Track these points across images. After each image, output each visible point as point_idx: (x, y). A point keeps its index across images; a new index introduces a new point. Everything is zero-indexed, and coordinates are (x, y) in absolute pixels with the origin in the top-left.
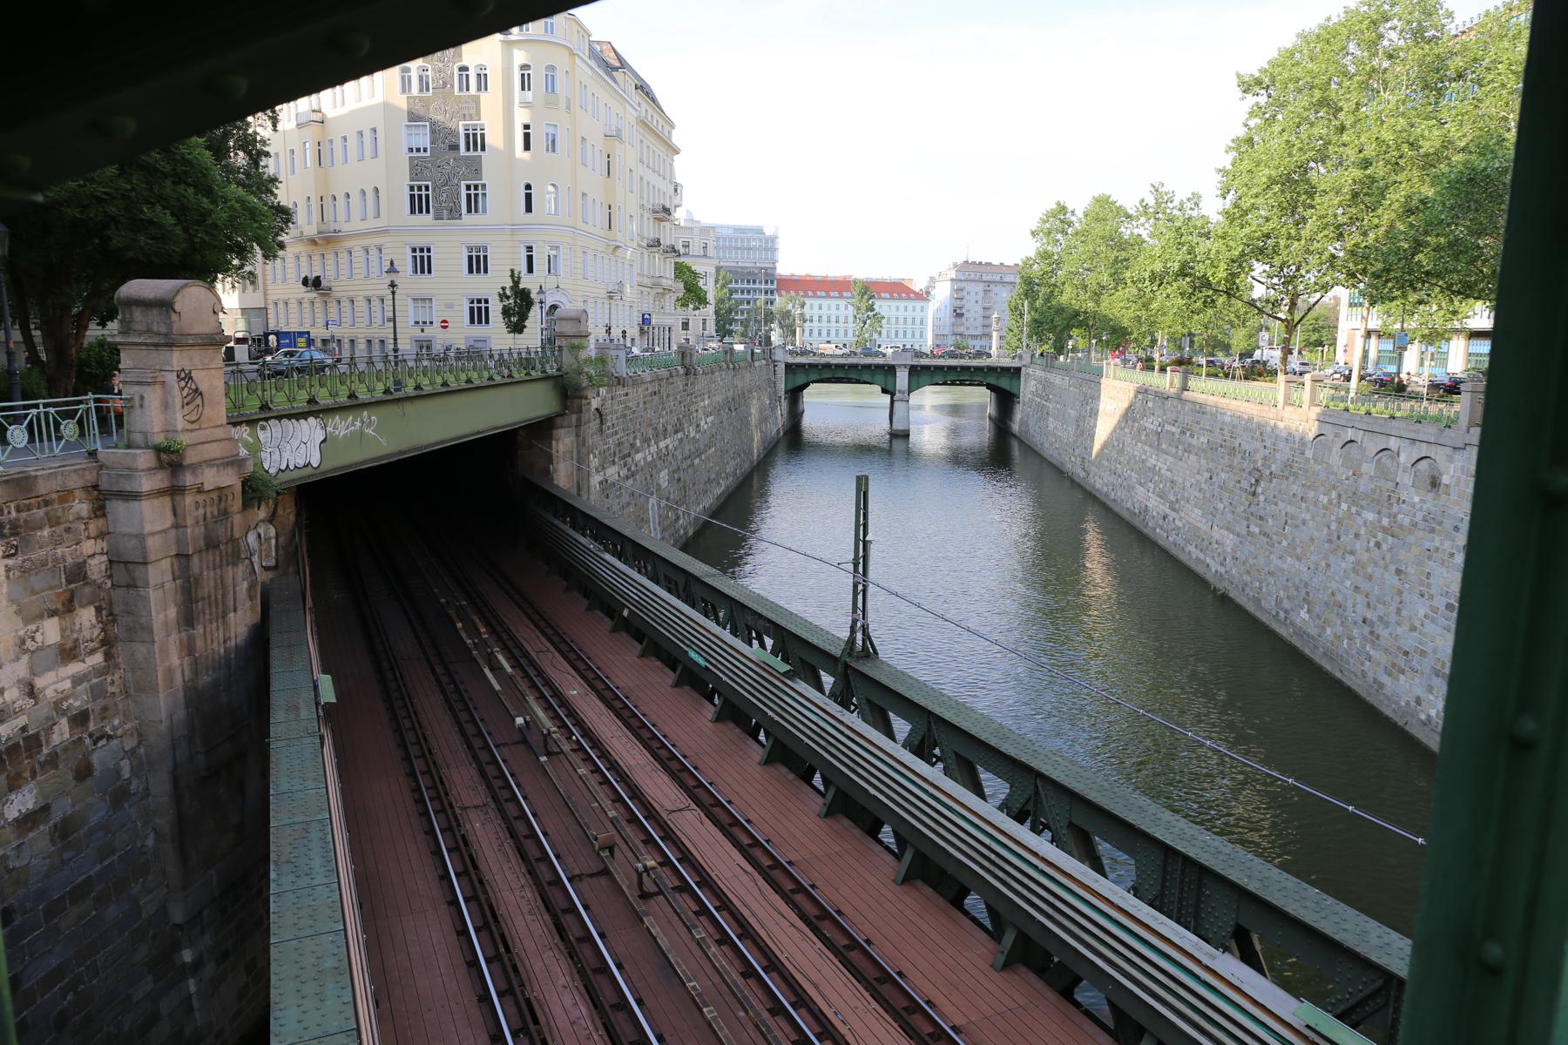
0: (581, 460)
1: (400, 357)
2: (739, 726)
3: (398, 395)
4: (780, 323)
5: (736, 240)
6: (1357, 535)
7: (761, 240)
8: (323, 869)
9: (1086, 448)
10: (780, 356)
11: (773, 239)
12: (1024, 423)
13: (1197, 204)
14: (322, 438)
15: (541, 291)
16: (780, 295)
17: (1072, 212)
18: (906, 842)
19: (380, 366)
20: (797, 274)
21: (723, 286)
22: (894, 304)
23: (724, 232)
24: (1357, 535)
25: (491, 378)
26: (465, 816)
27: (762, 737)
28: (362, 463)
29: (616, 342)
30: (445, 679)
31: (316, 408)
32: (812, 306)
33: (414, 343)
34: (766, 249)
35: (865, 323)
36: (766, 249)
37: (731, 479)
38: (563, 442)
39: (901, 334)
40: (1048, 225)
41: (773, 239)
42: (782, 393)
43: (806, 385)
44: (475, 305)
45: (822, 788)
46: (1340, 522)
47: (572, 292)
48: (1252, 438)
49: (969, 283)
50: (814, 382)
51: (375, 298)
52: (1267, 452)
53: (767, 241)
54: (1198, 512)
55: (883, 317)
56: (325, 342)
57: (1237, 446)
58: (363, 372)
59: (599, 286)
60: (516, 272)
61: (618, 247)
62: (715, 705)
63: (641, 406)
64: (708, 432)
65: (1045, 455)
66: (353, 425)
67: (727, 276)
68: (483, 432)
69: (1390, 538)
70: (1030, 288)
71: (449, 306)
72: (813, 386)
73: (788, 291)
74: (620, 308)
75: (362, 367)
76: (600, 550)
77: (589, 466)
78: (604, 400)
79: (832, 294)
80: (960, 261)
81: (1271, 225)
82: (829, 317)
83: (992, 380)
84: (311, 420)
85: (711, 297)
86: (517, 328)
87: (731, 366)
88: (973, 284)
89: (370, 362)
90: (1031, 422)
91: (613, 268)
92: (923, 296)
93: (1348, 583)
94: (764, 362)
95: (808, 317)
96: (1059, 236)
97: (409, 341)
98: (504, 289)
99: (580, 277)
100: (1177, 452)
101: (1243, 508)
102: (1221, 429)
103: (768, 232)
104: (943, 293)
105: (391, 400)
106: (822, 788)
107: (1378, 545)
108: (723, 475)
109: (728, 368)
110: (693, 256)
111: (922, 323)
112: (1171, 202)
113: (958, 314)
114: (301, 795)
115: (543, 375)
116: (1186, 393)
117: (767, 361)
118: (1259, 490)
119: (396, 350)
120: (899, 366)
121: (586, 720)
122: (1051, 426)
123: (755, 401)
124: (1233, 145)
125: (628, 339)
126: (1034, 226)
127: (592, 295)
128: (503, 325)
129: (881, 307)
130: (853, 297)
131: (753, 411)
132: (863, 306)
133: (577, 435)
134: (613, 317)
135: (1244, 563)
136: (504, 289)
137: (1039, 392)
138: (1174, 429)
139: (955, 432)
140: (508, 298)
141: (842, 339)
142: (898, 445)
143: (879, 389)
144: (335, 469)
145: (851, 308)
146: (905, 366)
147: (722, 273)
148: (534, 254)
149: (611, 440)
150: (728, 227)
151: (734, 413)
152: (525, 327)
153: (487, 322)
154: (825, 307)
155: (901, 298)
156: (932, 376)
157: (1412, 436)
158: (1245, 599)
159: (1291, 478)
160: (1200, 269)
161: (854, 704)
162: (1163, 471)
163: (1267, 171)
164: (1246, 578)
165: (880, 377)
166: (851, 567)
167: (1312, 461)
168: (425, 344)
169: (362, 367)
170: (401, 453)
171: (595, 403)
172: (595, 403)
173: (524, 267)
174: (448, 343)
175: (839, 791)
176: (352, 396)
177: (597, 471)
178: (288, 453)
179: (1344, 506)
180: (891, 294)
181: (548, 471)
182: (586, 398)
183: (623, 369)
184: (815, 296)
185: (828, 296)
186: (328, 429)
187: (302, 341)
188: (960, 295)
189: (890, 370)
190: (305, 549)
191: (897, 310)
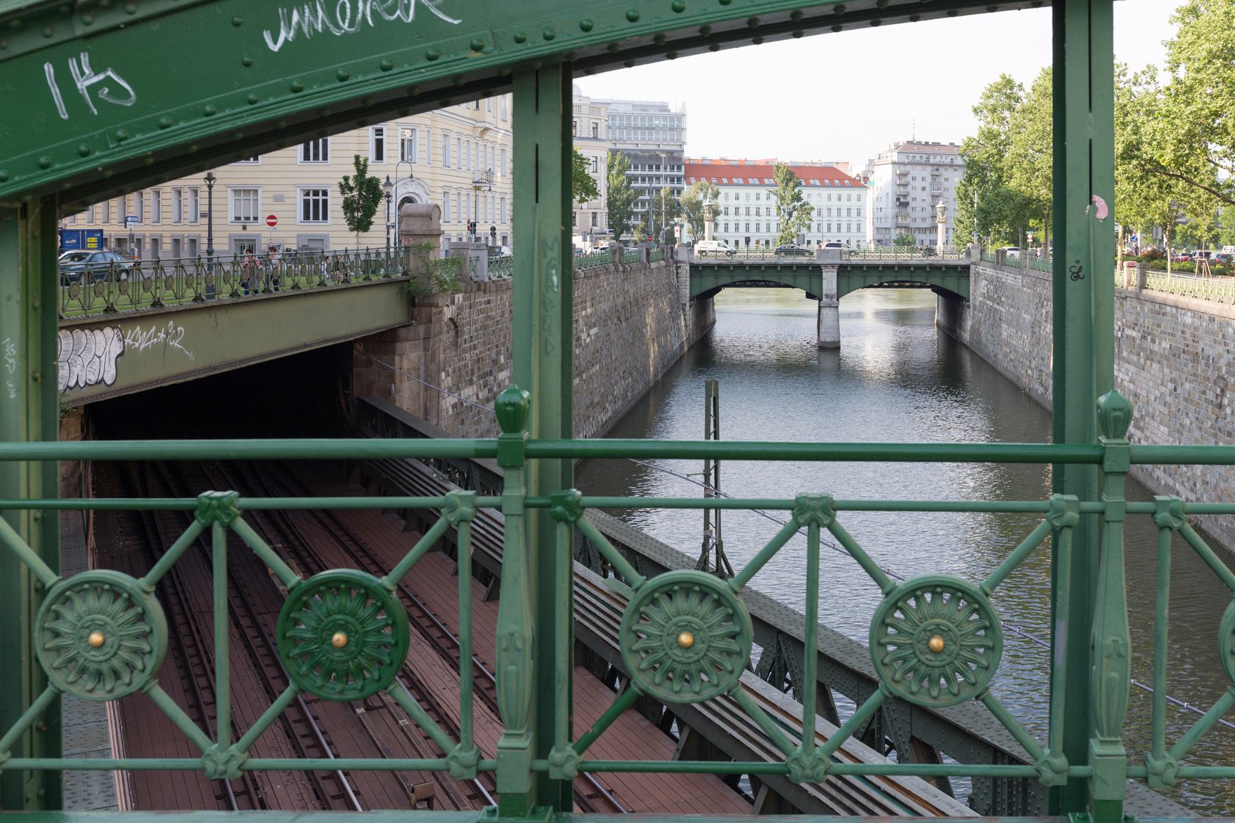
0: (430, 379)
1: (215, 260)
2: (592, 672)
3: (210, 303)
4: (689, 216)
5: (636, 118)
7: (665, 119)
8: (102, 794)
9: (1043, 359)
10: (682, 255)
11: (680, 117)
12: (975, 331)
13: (1153, 78)
14: (119, 351)
15: (388, 184)
16: (689, 183)
17: (1020, 86)
18: (685, 723)
19: (190, 270)
20: (692, 157)
21: (620, 173)
22: (825, 192)
23: (621, 109)
25: (322, 284)
26: (264, 778)
27: (675, 728)
28: (165, 380)
29: (483, 241)
30: (260, 652)
31: (114, 317)
32: (727, 195)
33: (233, 244)
35: (790, 215)
36: (671, 129)
37: (620, 402)
38: (408, 357)
39: (834, 228)
40: (992, 101)
41: (680, 117)
42: (686, 300)
43: (717, 290)
44: (311, 197)
45: (750, 793)
47: (429, 182)
48: (1215, 341)
49: (914, 167)
51: (186, 189)
53: (672, 119)
54: (1164, 429)
55: (812, 209)
56: (120, 241)
57: (1199, 350)
58: (170, 276)
59: (464, 175)
60: (361, 159)
61: (486, 129)
62: (615, 690)
63: (507, 315)
64: (591, 347)
65: (999, 369)
66: (156, 336)
67: (622, 160)
68: (310, 345)
70: (975, 170)
71: (279, 199)
72: (726, 291)
73: (698, 179)
74: (490, 200)
75: (170, 271)
76: (444, 480)
77: (439, 386)
78: (460, 308)
79: (735, 180)
80: (902, 140)
81: (1220, 102)
82: (748, 209)
83: (936, 281)
84: (108, 331)
85: (602, 187)
86: (361, 225)
88: (919, 167)
89: (179, 266)
90: (983, 330)
91: (481, 154)
92: (859, 183)
94: (663, 263)
95: (722, 209)
96: (1007, 114)
97: (227, 241)
98: (346, 179)
99: (440, 165)
100: (1139, 361)
101: (1210, 423)
102: (1183, 332)
103: (674, 109)
104: (884, 178)
105: (203, 307)
106: (750, 793)
108: (610, 398)
109: (617, 270)
111: (859, 214)
112: (1124, 75)
113: (902, 203)
114: (80, 728)
115: (386, 280)
116: (1144, 291)
117: (667, 261)
118: (1226, 401)
119: (210, 252)
120: (826, 266)
121: (415, 671)
122: (1005, 334)
123: (651, 309)
124: (1178, 15)
125: (499, 237)
126: (977, 101)
127: (455, 186)
128: (344, 221)
129: (809, 195)
130: (776, 185)
131: (649, 320)
132: (788, 195)
133: (426, 350)
134: (481, 211)
135: (1215, 487)
136: (346, 179)
137: (991, 294)
138: (1134, 334)
139: (901, 348)
140: (351, 189)
141: (764, 235)
142: (828, 361)
143: (803, 293)
144: (133, 387)
145: (773, 198)
146: (833, 265)
147: (618, 158)
148: (385, 138)
149: (468, 356)
150: (626, 103)
151: (624, 324)
152: (371, 223)
153: (325, 217)
154: (844, 198)
155: (833, 186)
156: (865, 278)
158: (1218, 531)
160: (1147, 151)
161: (787, 681)
162: (1125, 383)
163: (1207, 46)
165: (803, 279)
166: (701, 479)
168: (246, 244)
169: (170, 271)
170: (210, 368)
171: (448, 312)
172: (448, 312)
173: (371, 154)
174: (275, 243)
175: (692, 731)
176: (157, 303)
177: (450, 390)
178: (79, 368)
180: (821, 180)
181: (389, 391)
182: (437, 306)
183: (484, 273)
184: (731, 184)
185: (746, 184)
186: (127, 341)
187: (92, 241)
188: (904, 181)
189: (815, 271)
190: (90, 479)
191: (840, 199)
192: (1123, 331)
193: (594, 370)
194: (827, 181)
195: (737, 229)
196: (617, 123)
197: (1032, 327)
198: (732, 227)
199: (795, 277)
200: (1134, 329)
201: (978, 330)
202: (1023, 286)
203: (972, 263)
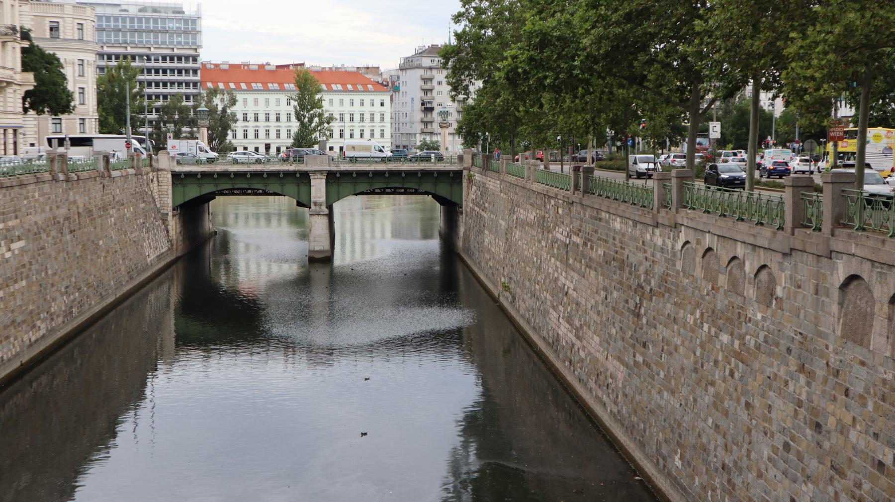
6: (716, 362)
24: (716, 362)
34: (186, 32)
36: (186, 32)
43: (211, 196)
46: (702, 346)
50: (221, 193)
52: (648, 264)
53: (186, 21)
69: (741, 364)
72: (219, 199)
82: (267, 115)
87: (61, 177)
93: (710, 421)
101: (630, 333)
103: (189, 10)
107: (732, 374)
109: (55, 179)
110: (65, 40)
120: (315, 172)
142: (320, 275)
146: (321, 172)
154: (367, 102)
155: (356, 90)
157: (751, 240)
159: (667, 295)
162: (570, 292)
164: (635, 419)
165: (291, 187)
167: (681, 274)
179: (706, 327)
184: (250, 90)
185: (266, 90)
188: (428, 86)
191: (362, 104)
192: (570, 238)
193: (17, 286)
194: (350, 87)
195: (256, 136)
196: (128, 25)
197: (506, 234)
198: (251, 134)
199: (282, 185)
200: (578, 235)
201: (469, 237)
202: (501, 192)
203: (465, 169)
